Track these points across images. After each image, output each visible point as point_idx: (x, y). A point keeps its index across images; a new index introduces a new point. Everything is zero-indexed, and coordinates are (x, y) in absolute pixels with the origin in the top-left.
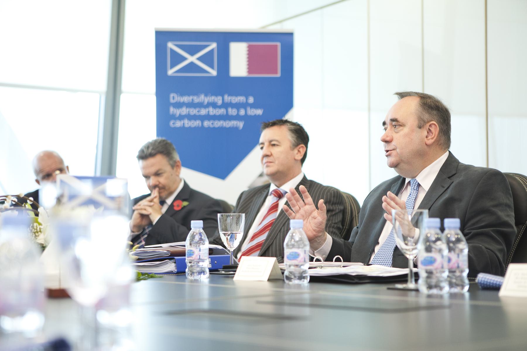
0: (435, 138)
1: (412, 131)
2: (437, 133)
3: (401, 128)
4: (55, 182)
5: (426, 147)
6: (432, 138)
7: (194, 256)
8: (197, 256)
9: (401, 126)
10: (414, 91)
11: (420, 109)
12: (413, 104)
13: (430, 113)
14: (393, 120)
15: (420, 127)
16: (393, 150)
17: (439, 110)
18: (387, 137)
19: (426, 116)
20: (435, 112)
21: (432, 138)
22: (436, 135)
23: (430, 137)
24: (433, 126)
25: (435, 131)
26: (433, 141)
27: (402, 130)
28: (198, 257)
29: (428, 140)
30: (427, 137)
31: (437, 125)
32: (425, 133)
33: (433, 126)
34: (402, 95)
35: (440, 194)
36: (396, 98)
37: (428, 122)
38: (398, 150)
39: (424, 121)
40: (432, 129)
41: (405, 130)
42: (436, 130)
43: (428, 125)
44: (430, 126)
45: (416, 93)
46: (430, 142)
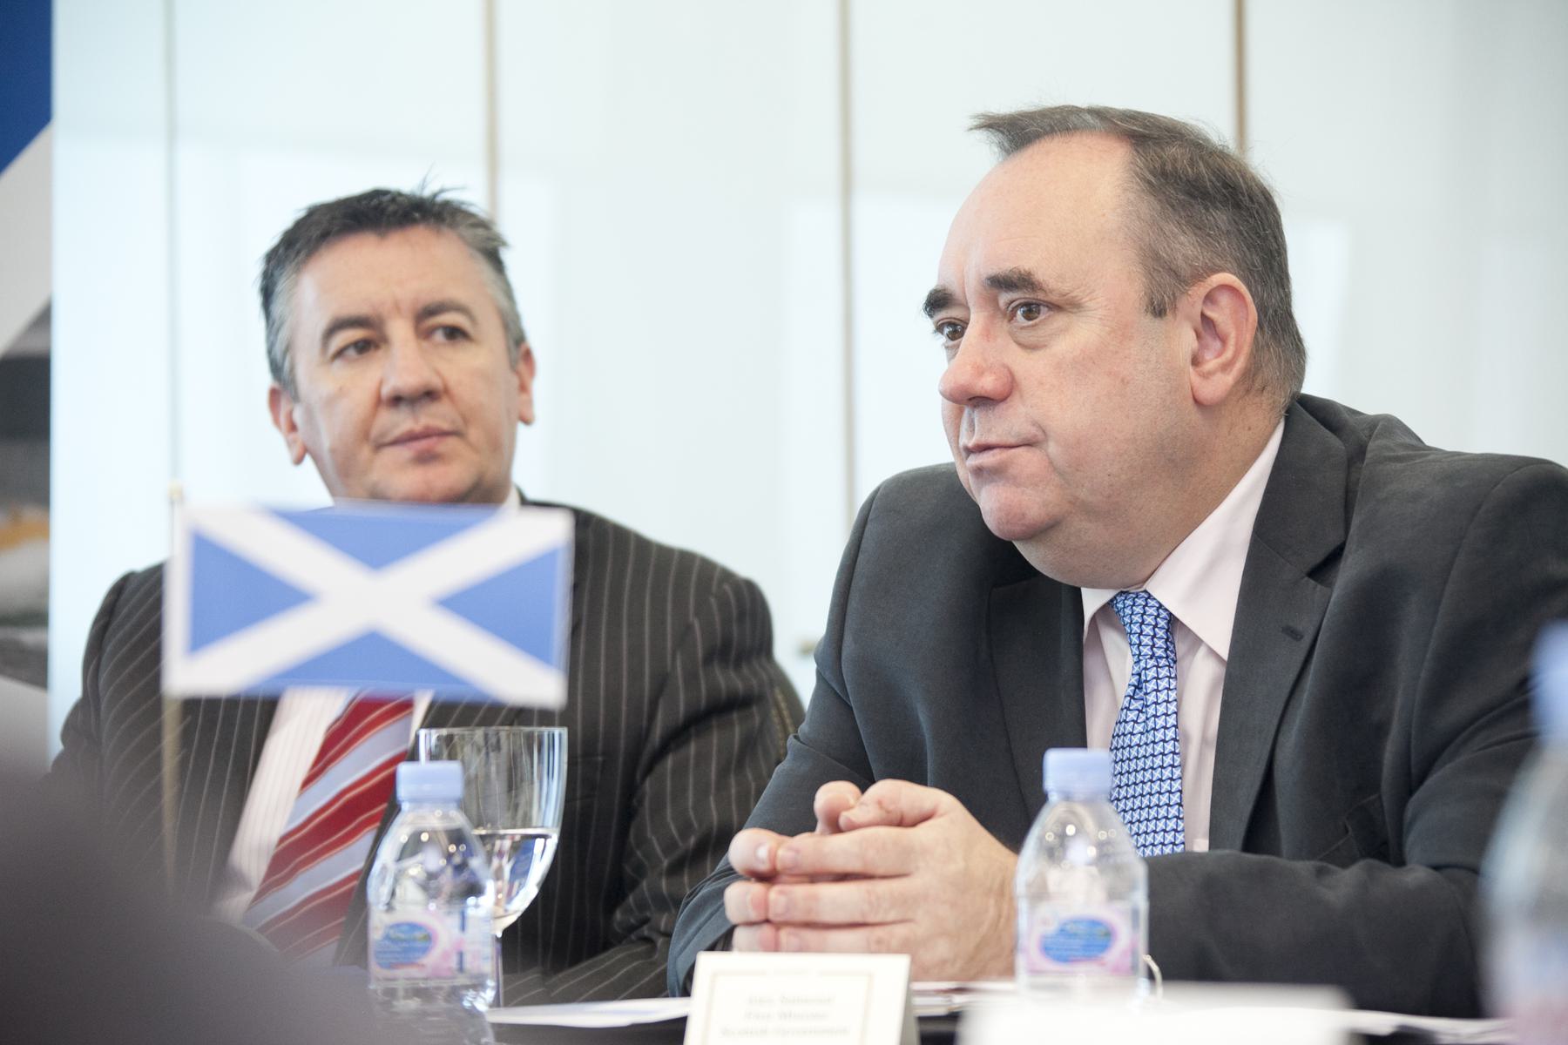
0: (1240, 364)
1: (1122, 332)
2: (1248, 337)
3: (1060, 320)
4: (954, 1017)
5: (1195, 416)
6: (1225, 367)
7: (432, 959)
8: (446, 955)
9: (1056, 307)
10: (1083, 103)
11: (1147, 206)
12: (1100, 180)
13: (1198, 228)
14: (1001, 283)
15: (1158, 310)
16: (1029, 444)
17: (1238, 205)
18: (980, 372)
19: (1184, 247)
20: (1221, 218)
21: (1225, 367)
22: (1246, 349)
23: (1211, 363)
24: (1224, 299)
25: (1238, 328)
26: (1229, 379)
27: (1064, 331)
28: (454, 963)
29: (1206, 376)
30: (1196, 361)
31: (1243, 289)
32: (1185, 339)
33: (1224, 299)
34: (1018, 132)
35: (1292, 676)
36: (985, 152)
37: (1199, 276)
38: (1053, 448)
39: (1175, 273)
40: (1221, 314)
41: (1074, 337)
42: (1238, 320)
43: (1200, 291)
44: (1209, 298)
45: (1101, 114)
46: (1217, 386)
